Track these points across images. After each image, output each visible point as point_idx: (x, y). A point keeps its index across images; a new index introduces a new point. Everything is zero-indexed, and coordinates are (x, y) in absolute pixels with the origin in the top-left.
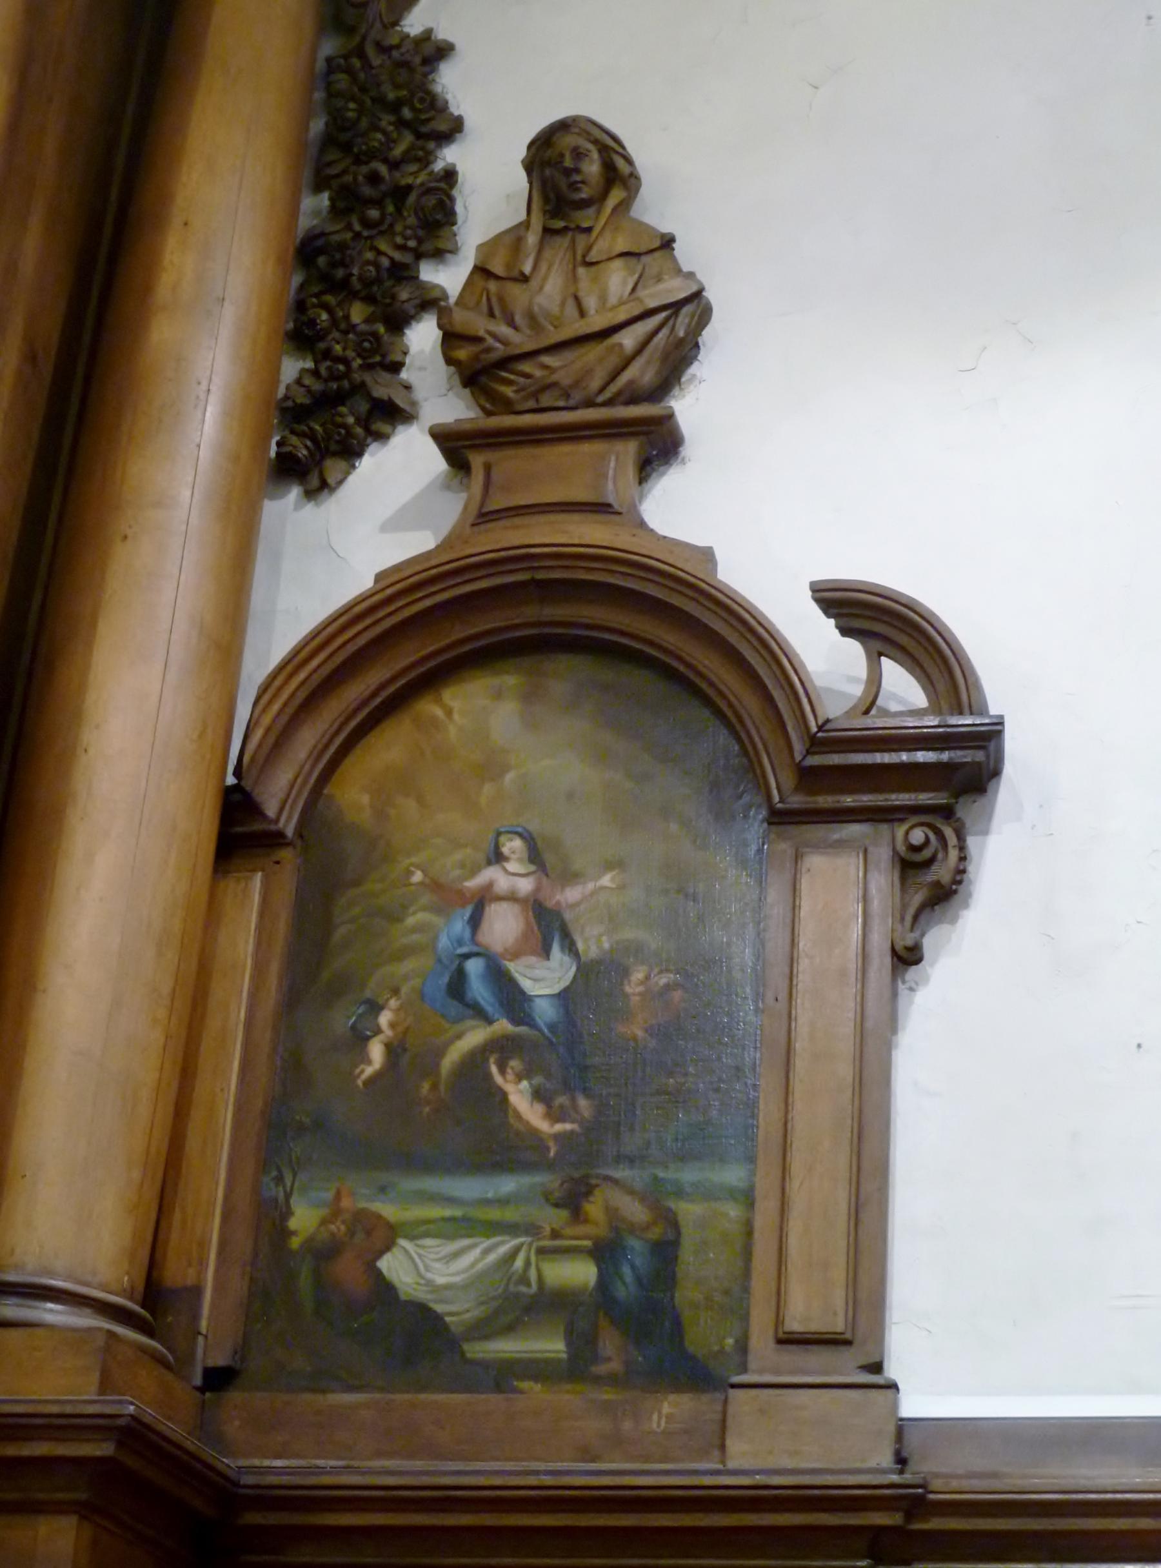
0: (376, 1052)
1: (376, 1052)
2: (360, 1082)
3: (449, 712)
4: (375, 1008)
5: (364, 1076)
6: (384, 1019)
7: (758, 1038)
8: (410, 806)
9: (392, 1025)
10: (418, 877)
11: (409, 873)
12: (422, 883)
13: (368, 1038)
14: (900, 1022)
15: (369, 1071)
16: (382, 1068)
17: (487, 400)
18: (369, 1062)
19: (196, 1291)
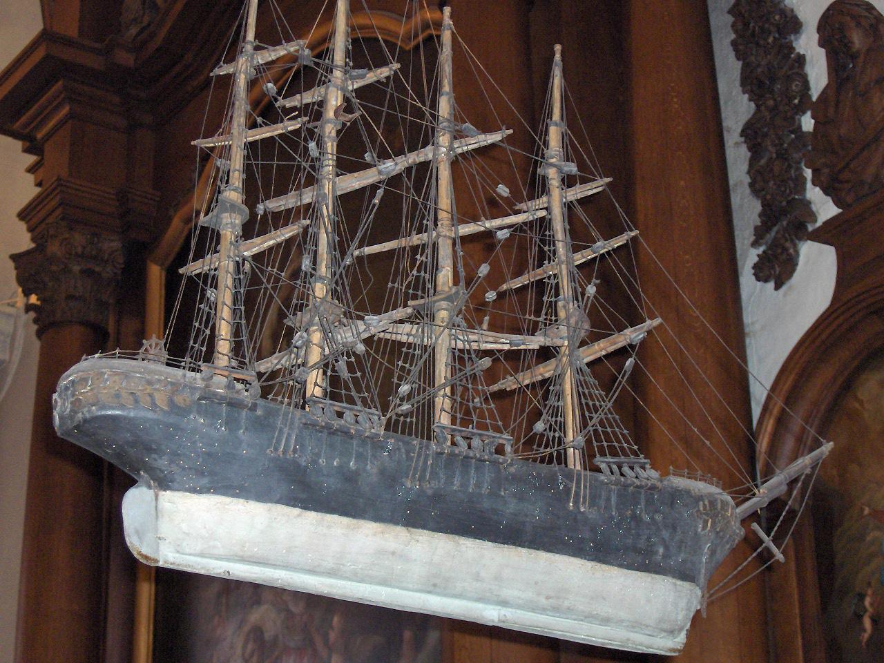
0: (867, 623)
1: (867, 623)
2: (863, 644)
3: (861, 403)
4: (862, 597)
5: (865, 640)
6: (867, 601)
7: (144, 195)
8: (854, 468)
9: (871, 604)
10: (867, 511)
11: (862, 510)
12: (870, 514)
13: (862, 616)
14: (740, 270)
15: (866, 636)
16: (872, 632)
17: (563, 247)
18: (865, 631)
19: (811, 458)
